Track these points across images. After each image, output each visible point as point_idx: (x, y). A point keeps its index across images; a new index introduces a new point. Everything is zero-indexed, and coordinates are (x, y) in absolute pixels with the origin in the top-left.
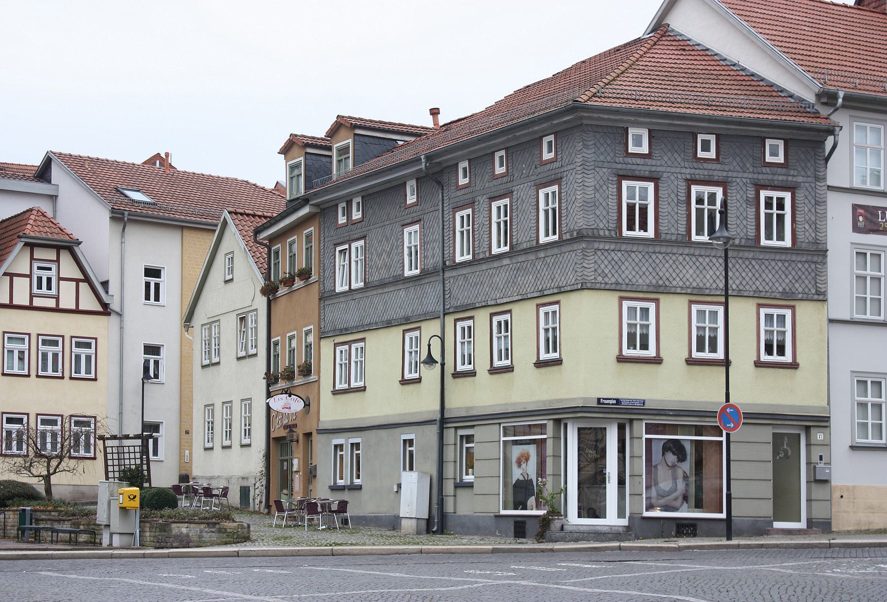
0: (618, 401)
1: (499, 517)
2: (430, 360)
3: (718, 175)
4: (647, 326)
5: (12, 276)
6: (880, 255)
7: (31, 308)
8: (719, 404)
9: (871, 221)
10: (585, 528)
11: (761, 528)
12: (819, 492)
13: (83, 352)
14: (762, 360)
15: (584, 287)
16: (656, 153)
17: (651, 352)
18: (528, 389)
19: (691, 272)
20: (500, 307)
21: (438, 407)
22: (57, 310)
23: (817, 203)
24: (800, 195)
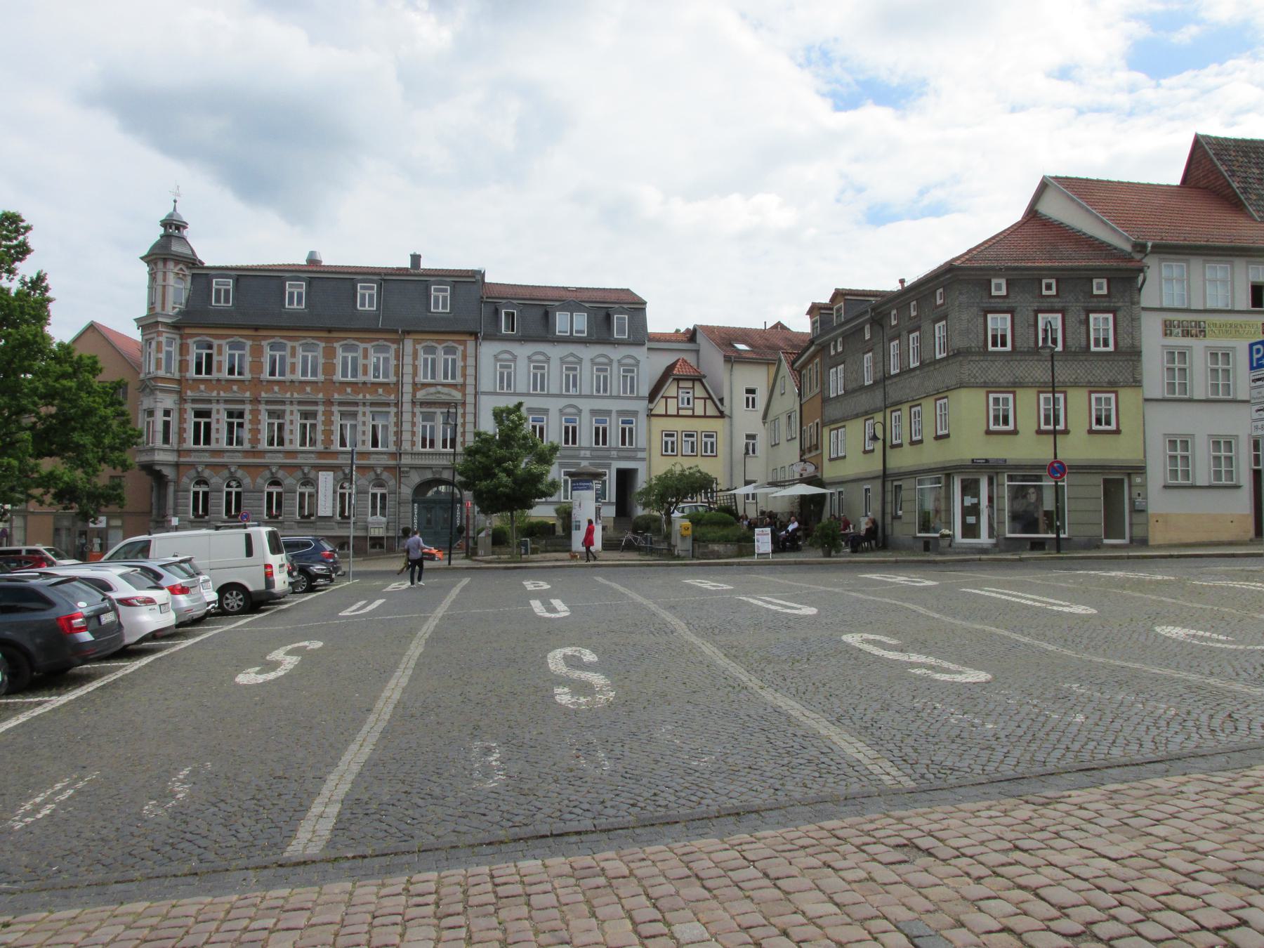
0: (987, 461)
1: (916, 538)
2: (875, 438)
3: (1058, 305)
5: (666, 398)
7: (678, 416)
11: (1094, 544)
12: (1138, 518)
13: (709, 440)
15: (961, 385)
16: (1012, 295)
17: (1011, 427)
18: (932, 454)
20: (915, 402)
22: (693, 416)
23: (1133, 320)
24: (1120, 315)
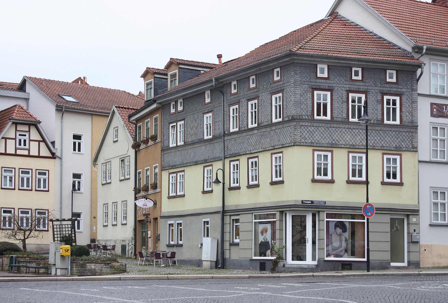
0: (312, 202)
1: (252, 260)
2: (217, 181)
3: (362, 88)
4: (327, 164)
5: (6, 139)
6: (444, 128)
7: (16, 155)
8: (363, 203)
9: (440, 111)
10: (295, 266)
11: (384, 266)
12: (414, 248)
13: (42, 177)
14: (385, 181)
15: (295, 144)
16: (331, 77)
17: (329, 177)
18: (267, 196)
19: (349, 137)
20: (252, 154)
21: (221, 205)
22: (29, 156)
23: (413, 102)
24: (404, 98)
